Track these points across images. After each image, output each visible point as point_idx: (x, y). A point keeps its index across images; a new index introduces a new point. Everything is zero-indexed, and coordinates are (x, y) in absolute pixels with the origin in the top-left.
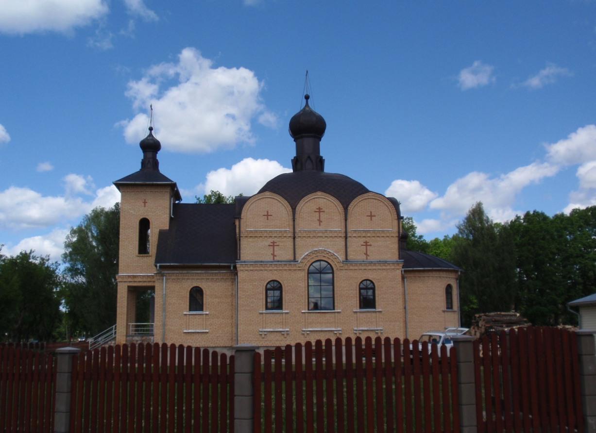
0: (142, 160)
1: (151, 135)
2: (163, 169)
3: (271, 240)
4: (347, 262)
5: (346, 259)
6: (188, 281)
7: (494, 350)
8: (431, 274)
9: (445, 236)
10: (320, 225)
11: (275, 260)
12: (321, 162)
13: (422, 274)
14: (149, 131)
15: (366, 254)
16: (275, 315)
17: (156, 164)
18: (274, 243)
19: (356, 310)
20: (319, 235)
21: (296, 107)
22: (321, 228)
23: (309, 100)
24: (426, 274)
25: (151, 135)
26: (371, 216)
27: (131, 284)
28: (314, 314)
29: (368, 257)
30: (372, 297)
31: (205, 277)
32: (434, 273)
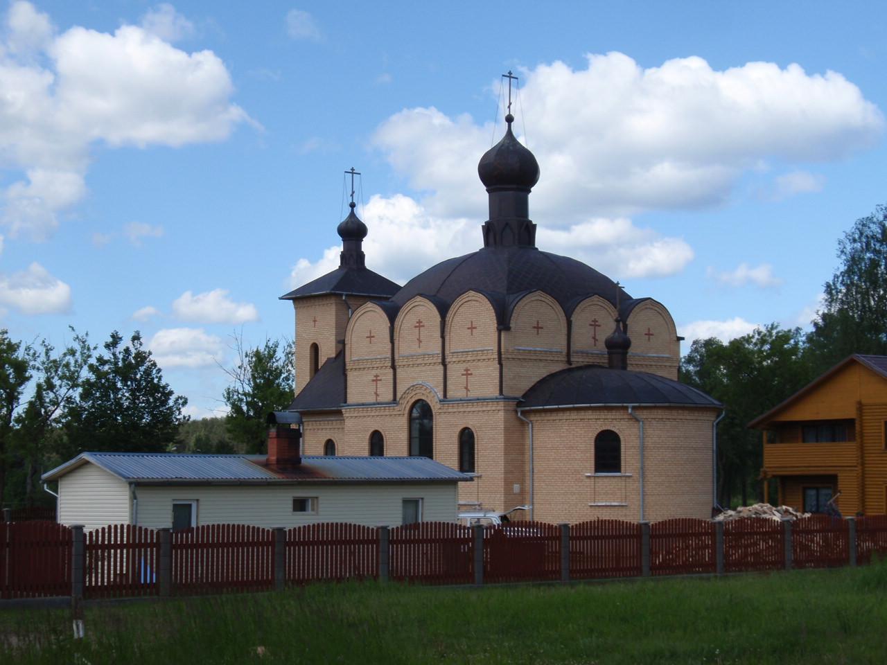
0: (342, 252)
1: (352, 215)
2: (549, 240)
3: (374, 372)
4: (394, 403)
5: (445, 395)
6: (324, 431)
7: (526, 531)
8: (567, 415)
9: (167, 384)
10: (419, 347)
11: (378, 401)
12: (530, 229)
13: (554, 416)
14: (350, 209)
15: (466, 388)
16: (608, 481)
17: (361, 257)
18: (377, 376)
19: (589, 474)
20: (420, 361)
21: (493, 137)
22: (420, 351)
23: (512, 124)
24: (560, 415)
25: (352, 215)
26: (472, 328)
27: (857, 422)
28: (616, 480)
29: (469, 393)
30: (167, 450)
31: (327, 427)
32: (568, 413)
